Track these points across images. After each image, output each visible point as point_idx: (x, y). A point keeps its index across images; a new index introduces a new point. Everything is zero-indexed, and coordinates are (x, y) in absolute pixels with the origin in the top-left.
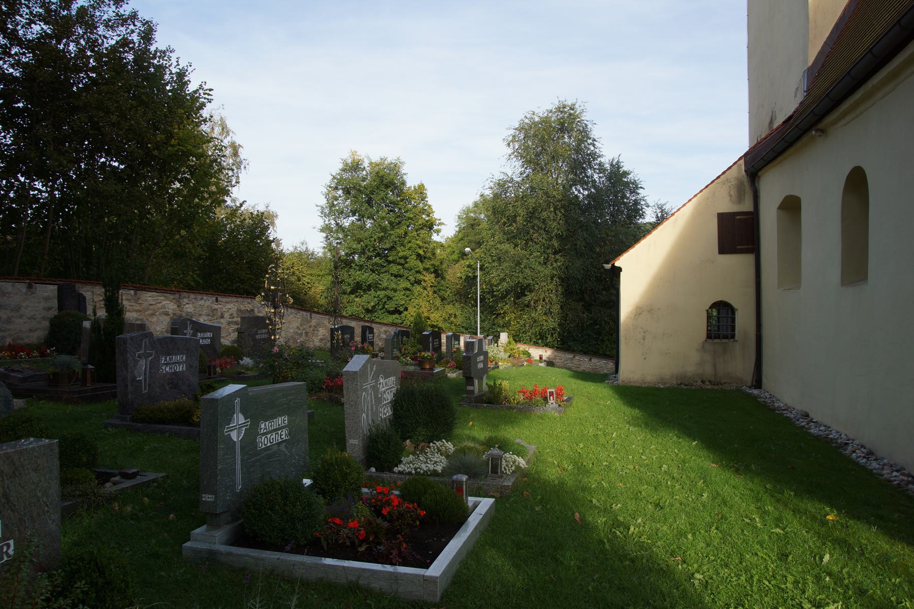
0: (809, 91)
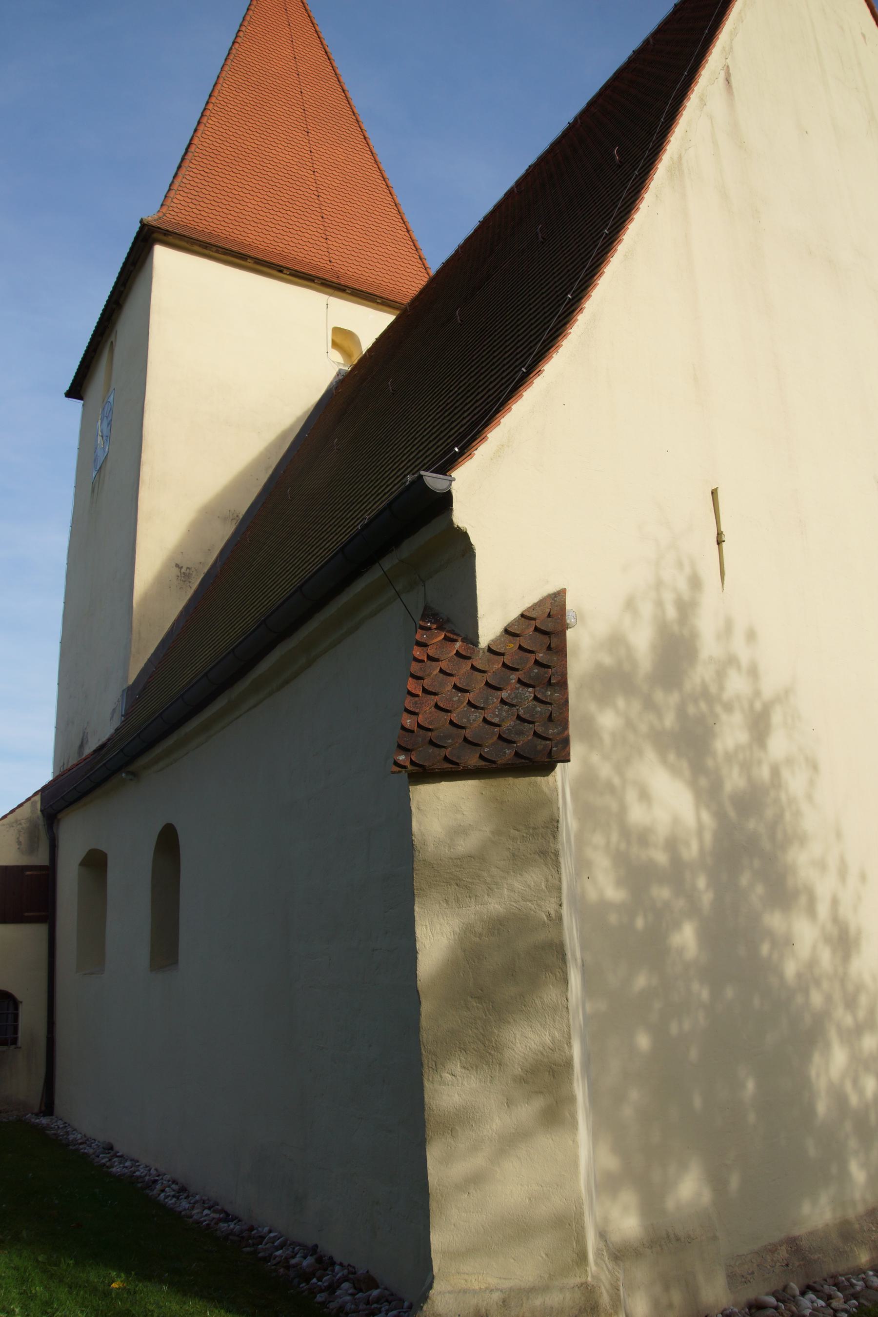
0: (127, 715)
